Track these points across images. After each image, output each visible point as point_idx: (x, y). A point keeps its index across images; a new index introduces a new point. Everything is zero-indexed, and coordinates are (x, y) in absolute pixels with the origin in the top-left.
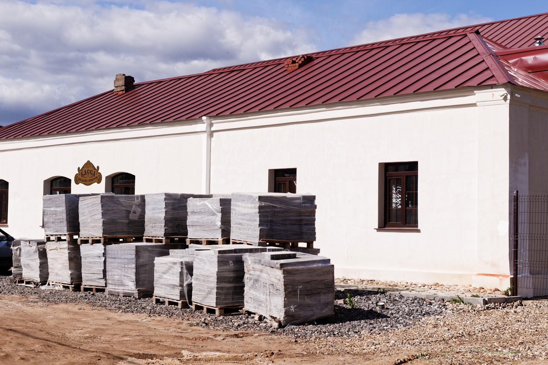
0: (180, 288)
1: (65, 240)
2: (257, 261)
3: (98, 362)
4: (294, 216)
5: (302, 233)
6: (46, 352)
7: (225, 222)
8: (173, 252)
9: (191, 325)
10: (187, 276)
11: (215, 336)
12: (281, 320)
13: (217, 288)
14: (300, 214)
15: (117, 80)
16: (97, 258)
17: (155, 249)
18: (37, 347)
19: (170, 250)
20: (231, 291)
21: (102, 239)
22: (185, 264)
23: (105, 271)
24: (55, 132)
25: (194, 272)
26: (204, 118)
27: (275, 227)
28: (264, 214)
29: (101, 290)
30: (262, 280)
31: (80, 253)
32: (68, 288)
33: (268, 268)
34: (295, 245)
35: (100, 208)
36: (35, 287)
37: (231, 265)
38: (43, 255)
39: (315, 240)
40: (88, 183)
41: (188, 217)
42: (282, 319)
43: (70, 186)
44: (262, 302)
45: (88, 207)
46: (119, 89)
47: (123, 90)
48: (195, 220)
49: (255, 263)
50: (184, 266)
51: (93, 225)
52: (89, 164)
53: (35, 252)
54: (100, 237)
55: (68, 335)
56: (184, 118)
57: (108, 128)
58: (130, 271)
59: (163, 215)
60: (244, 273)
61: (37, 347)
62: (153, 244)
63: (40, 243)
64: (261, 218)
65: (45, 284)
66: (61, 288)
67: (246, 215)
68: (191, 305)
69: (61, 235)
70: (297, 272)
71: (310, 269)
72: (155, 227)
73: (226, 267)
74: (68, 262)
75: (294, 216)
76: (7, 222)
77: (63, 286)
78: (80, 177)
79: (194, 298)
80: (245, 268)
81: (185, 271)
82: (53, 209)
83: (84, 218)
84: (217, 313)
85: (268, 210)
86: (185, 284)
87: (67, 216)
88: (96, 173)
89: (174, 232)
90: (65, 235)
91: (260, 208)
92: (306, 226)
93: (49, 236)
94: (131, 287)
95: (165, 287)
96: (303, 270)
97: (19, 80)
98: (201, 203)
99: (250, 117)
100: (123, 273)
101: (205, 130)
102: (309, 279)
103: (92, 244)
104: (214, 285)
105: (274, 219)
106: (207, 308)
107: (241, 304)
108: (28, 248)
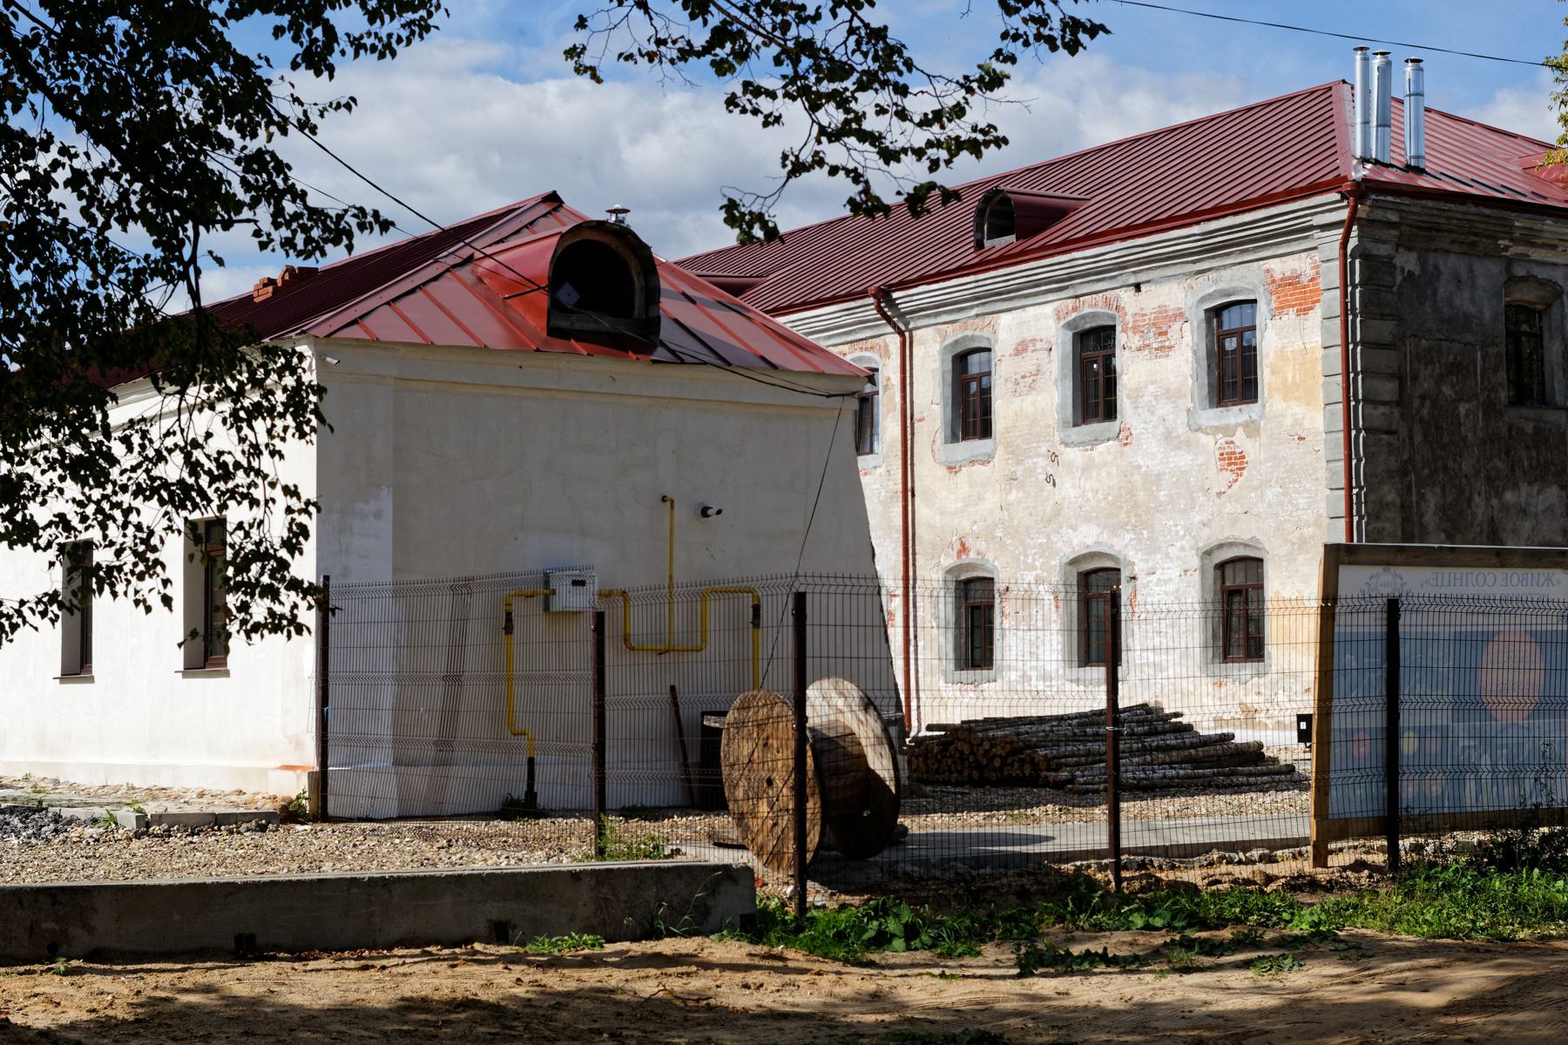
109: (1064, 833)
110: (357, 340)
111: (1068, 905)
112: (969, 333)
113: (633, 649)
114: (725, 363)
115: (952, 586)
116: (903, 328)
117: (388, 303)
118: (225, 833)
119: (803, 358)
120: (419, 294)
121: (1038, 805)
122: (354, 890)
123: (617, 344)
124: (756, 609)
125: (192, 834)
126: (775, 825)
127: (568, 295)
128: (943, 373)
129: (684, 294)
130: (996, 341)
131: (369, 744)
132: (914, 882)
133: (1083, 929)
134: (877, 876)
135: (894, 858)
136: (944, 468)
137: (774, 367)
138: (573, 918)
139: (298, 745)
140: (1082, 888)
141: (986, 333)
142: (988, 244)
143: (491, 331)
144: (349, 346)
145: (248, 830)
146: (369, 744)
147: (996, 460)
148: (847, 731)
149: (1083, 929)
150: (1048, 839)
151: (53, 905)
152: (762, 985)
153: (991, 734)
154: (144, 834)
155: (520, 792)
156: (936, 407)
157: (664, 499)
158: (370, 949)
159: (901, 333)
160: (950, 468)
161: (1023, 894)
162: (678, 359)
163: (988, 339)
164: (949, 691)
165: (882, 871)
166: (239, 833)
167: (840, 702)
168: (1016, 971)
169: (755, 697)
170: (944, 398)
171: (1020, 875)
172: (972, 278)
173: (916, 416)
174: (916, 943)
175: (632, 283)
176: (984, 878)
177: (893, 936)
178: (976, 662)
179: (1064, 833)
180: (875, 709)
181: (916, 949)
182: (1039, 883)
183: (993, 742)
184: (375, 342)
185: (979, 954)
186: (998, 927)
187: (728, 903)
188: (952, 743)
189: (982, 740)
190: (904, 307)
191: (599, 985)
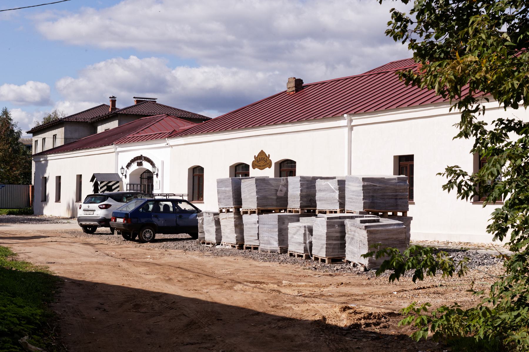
0: (304, 245)
1: (232, 212)
2: (352, 225)
3: (224, 284)
4: (391, 192)
5: (397, 205)
6: (195, 279)
7: (342, 197)
8: (302, 219)
9: (304, 269)
10: (309, 236)
11: (315, 275)
12: (366, 266)
13: (327, 244)
14: (396, 191)
15: (289, 82)
16: (254, 224)
17: (292, 218)
18: (191, 276)
19: (300, 218)
20: (337, 246)
21: (257, 211)
22: (308, 228)
23: (258, 234)
24: (237, 128)
25: (314, 233)
26: (345, 115)
27: (376, 201)
28: (367, 191)
29: (256, 248)
30: (356, 238)
31: (242, 221)
32: (235, 247)
33: (358, 229)
34: (395, 214)
35: (255, 188)
36: (212, 247)
37: (337, 228)
38: (218, 223)
39: (408, 210)
40: (262, 168)
41: (317, 194)
42: (367, 265)
43: (249, 170)
44: (355, 253)
45: (247, 187)
46: (290, 90)
47: (294, 91)
48: (321, 196)
49: (351, 226)
50: (307, 229)
51: (250, 200)
52: (262, 153)
53: (212, 221)
54: (255, 209)
55: (216, 272)
56: (330, 116)
57: (275, 124)
58: (274, 234)
59: (299, 193)
60: (345, 233)
61: (191, 276)
62: (293, 214)
63: (215, 214)
64: (364, 194)
65: (219, 244)
66: (230, 247)
67: (355, 192)
68: (312, 257)
69: (229, 208)
70: (377, 232)
71: (388, 230)
72: (294, 201)
73: (333, 229)
74: (234, 228)
75: (391, 192)
76: (203, 200)
77: (231, 246)
78: (256, 163)
79: (313, 252)
80: (346, 230)
81: (307, 233)
82: (223, 189)
83: (245, 195)
84: (327, 261)
85: (369, 188)
86: (307, 242)
87: (233, 194)
88: (267, 160)
89: (307, 205)
90: (232, 208)
91: (363, 186)
92: (400, 200)
93: (221, 209)
94: (275, 245)
95: (295, 244)
96: (382, 230)
97: (234, 69)
98: (325, 183)
99: (379, 115)
100: (270, 235)
101: (346, 125)
102: (387, 237)
103: (250, 214)
104: (325, 242)
105: (375, 195)
106: (321, 259)
107: (344, 256)
108: (208, 218)
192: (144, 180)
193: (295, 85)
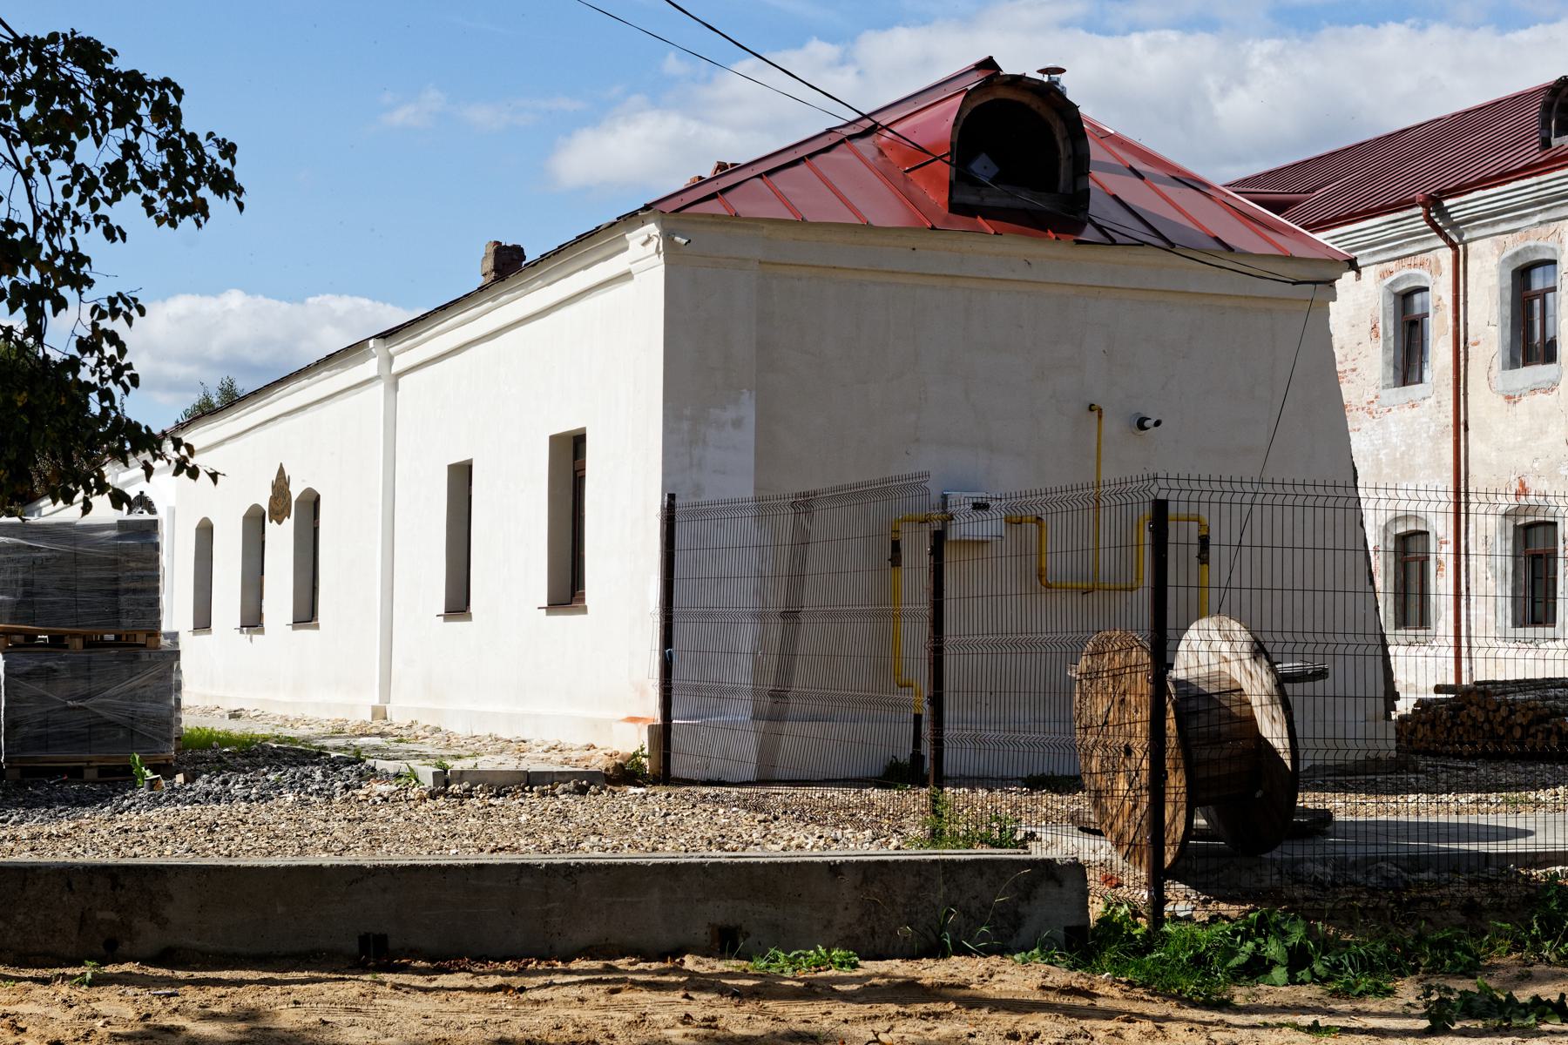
76: (583, 600)
99: (424, 335)
109: (1550, 826)
110: (713, 216)
111: (1530, 927)
112: (1532, 243)
113: (1049, 586)
114: (1170, 246)
115: (1510, 533)
116: (1456, 240)
117: (759, 176)
118: (535, 795)
119: (1272, 243)
120: (802, 168)
121: (1545, 786)
122: (526, 880)
123: (1034, 222)
124: (1204, 542)
125: (498, 796)
126: (1135, 807)
127: (983, 167)
128: (1501, 289)
129: (1131, 169)
130: (1563, 251)
131: (724, 693)
132: (1325, 889)
133: (1549, 962)
134: (1271, 879)
135: (1298, 854)
136: (1501, 398)
137: (1230, 249)
138: (828, 925)
139: (643, 693)
140: (1553, 905)
141: (1552, 242)
142: (1555, 142)
143: (884, 209)
144: (702, 222)
145: (565, 792)
146: (724, 693)
147: (1561, 387)
148: (1234, 686)
149: (1549, 962)
150: (1527, 833)
151: (113, 888)
152: (1037, 1035)
153: (1510, 697)
154: (440, 793)
155: (905, 756)
156: (1493, 329)
157: (1091, 408)
158: (540, 959)
159: (1453, 246)
160: (1508, 398)
161: (1471, 909)
162: (1109, 239)
163: (1553, 249)
164: (1507, 651)
165: (1280, 872)
166: (554, 795)
167: (1225, 647)
168: (1425, 1024)
169: (1109, 638)
170: (1502, 318)
171: (1471, 883)
172: (1534, 180)
173: (1470, 340)
174: (1304, 974)
175: (1058, 152)
176: (1419, 884)
177: (1273, 963)
178: (1536, 619)
179: (1550, 826)
180: (1268, 659)
181: (1303, 983)
182: (1494, 894)
183: (1512, 708)
184: (735, 218)
185: (1390, 992)
186: (1424, 955)
187: (1046, 911)
188: (1463, 708)
189: (1499, 706)
190: (1457, 216)
191: (802, 1027)
192: (1123, 582)
193: (495, 266)
